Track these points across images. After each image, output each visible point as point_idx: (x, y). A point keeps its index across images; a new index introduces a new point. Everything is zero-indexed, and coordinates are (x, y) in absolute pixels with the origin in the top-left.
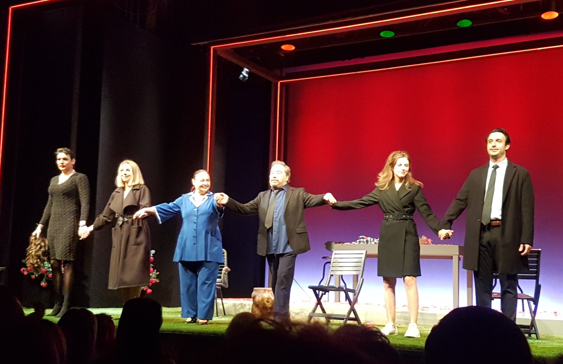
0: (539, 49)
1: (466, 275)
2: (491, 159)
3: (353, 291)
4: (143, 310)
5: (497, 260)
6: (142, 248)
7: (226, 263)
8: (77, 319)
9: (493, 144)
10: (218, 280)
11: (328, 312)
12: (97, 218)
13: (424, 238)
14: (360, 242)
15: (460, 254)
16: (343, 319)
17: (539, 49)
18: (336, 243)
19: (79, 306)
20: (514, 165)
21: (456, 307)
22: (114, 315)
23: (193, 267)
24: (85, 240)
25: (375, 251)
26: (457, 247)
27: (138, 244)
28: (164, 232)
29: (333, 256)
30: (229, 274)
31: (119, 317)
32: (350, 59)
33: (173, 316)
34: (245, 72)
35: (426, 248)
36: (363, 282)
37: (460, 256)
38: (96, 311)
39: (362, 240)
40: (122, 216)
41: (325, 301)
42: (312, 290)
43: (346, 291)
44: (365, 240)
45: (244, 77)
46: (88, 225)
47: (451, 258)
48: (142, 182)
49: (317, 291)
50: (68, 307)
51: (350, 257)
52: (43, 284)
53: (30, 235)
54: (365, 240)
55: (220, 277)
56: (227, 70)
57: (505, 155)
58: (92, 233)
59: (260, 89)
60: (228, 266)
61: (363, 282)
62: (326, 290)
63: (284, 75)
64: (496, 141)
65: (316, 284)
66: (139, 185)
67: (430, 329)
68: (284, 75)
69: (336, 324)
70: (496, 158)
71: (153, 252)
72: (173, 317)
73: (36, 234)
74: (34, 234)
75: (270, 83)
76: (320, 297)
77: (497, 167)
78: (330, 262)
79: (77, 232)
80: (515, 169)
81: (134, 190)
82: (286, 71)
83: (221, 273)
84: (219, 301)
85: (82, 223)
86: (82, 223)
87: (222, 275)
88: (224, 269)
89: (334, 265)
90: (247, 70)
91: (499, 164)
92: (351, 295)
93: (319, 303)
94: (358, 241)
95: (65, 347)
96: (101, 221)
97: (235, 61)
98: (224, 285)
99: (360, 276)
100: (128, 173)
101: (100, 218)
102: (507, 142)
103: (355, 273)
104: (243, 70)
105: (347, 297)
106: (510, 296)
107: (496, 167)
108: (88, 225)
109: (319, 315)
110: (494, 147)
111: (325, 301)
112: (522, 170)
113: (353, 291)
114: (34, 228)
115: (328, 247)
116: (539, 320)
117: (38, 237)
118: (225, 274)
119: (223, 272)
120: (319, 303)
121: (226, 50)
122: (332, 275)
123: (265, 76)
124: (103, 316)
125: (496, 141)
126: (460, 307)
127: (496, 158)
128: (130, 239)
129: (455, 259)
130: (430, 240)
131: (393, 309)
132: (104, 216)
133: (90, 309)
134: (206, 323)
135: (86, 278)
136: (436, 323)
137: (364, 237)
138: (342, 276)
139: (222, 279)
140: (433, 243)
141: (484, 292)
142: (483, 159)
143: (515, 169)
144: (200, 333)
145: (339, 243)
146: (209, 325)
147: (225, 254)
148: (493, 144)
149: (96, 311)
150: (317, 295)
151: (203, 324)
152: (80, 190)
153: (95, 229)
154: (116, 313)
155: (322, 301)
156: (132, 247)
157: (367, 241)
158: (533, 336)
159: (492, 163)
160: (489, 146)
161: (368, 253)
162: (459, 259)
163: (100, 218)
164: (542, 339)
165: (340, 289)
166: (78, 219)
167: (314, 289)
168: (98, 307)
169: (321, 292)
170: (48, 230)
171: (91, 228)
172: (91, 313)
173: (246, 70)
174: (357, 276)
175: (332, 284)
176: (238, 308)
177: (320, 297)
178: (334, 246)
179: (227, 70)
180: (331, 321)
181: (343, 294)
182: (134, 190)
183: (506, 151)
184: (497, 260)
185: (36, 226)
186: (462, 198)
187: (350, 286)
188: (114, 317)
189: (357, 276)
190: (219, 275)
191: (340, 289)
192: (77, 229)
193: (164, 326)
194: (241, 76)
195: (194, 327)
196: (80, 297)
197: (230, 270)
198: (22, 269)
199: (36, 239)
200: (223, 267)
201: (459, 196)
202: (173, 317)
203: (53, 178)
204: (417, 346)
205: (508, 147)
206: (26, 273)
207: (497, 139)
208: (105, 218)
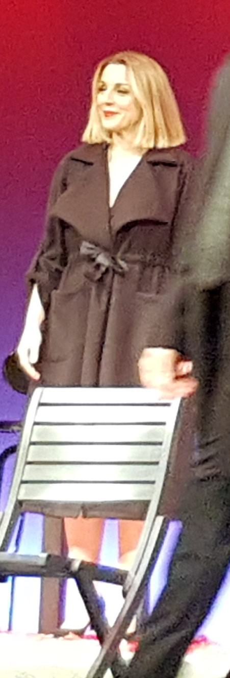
29: (33, 413)
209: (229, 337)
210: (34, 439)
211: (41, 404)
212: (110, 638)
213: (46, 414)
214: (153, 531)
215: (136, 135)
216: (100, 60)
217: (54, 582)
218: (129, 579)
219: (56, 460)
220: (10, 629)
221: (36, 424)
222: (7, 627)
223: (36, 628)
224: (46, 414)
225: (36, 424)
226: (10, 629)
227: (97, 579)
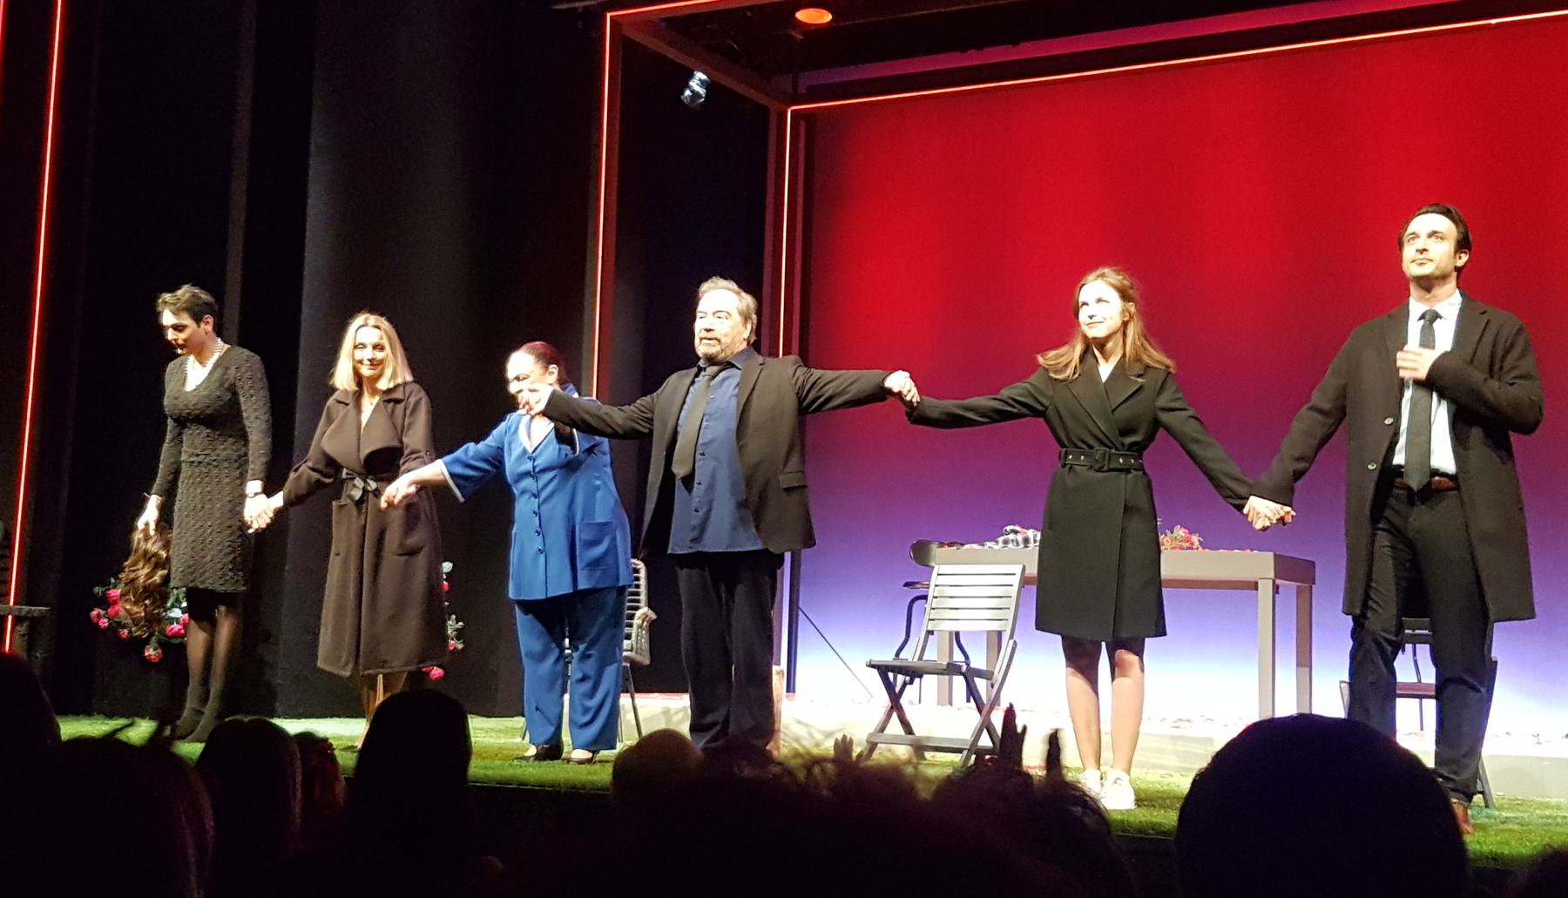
0: (1494, 21)
1: (1294, 633)
2: (1413, 290)
3: (987, 675)
4: (422, 729)
5: (1428, 586)
6: (421, 559)
7: (643, 597)
8: (248, 749)
9: (1419, 243)
10: (626, 644)
11: (919, 731)
12: (292, 475)
13: (1180, 532)
14: (1006, 542)
15: (1278, 575)
16: (959, 751)
17: (1494, 21)
18: (942, 545)
19: (249, 713)
20: (1482, 306)
21: (1267, 715)
22: (340, 738)
23: (557, 616)
24: (260, 534)
25: (1033, 570)
26: (1269, 557)
27: (412, 553)
28: (475, 517)
29: (934, 580)
30: (653, 628)
31: (359, 744)
32: (980, 48)
33: (502, 741)
34: (697, 83)
35: (1181, 556)
36: (1014, 650)
37: (1278, 582)
38: (293, 726)
39: (1011, 536)
40: (360, 475)
41: (911, 703)
42: (875, 671)
43: (970, 675)
44: (1020, 537)
45: (695, 94)
46: (269, 491)
47: (1255, 586)
48: (409, 378)
49: (891, 675)
50: (220, 716)
51: (982, 583)
52: (151, 652)
53: (132, 529)
54: (1020, 537)
55: (628, 637)
56: (650, 78)
57: (1452, 283)
58: (279, 514)
59: (737, 128)
60: (650, 606)
61: (1014, 650)
62: (914, 673)
63: (802, 90)
64: (1430, 241)
65: (887, 657)
66: (405, 384)
67: (1190, 780)
68: (802, 90)
69: (941, 765)
70: (1427, 284)
71: (447, 567)
72: (498, 742)
73: (147, 524)
74: (140, 524)
75: (765, 111)
76: (897, 689)
77: (1436, 316)
78: (925, 597)
79: (241, 513)
80: (1485, 318)
81: (389, 401)
82: (809, 79)
83: (631, 626)
84: (625, 700)
85: (253, 486)
86: (253, 486)
87: (634, 631)
88: (638, 613)
89: (935, 603)
90: (704, 77)
91: (1438, 308)
92: (981, 684)
93: (896, 705)
94: (1001, 539)
95: (210, 824)
96: (304, 482)
97: (672, 54)
98: (638, 658)
99: (1006, 636)
100: (379, 355)
101: (303, 472)
102: (1462, 245)
103: (995, 626)
104: (691, 76)
105: (972, 692)
106: (1464, 692)
107: (1431, 318)
108: (269, 491)
109: (895, 741)
110: (1423, 251)
111: (911, 703)
112: (1506, 321)
113: (987, 675)
114: (140, 507)
115: (921, 554)
116: (1492, 757)
117: (152, 533)
118: (640, 627)
119: (636, 622)
120: (896, 705)
121: (647, 24)
122: (931, 632)
123: (752, 94)
124: (307, 739)
125: (1430, 241)
126: (1278, 715)
127: (1427, 284)
128: (387, 537)
129: (1265, 589)
130: (1195, 539)
131: (1094, 729)
132: (313, 470)
133: (278, 722)
134: (589, 761)
135: (267, 637)
136: (1204, 763)
137: (1018, 528)
138: (957, 634)
139: (635, 643)
140: (1204, 545)
141: (1372, 684)
142: (1389, 291)
143: (1485, 318)
144: (574, 787)
145: (951, 545)
146: (598, 766)
147: (643, 574)
148: (1419, 243)
149: (293, 726)
150: (889, 686)
151: (581, 762)
152: (242, 399)
153: (289, 503)
154: (346, 733)
155: (903, 701)
156: (391, 560)
157: (1026, 541)
158: (1478, 798)
159: (1416, 307)
160: (1409, 252)
161: (1027, 571)
162: (1276, 589)
163: (303, 472)
164: (1501, 808)
165: (952, 669)
166: (242, 479)
167: (883, 670)
168: (299, 716)
169: (900, 678)
170: (176, 508)
171: (278, 500)
172: (281, 732)
173: (700, 75)
174: (1000, 633)
175: (931, 655)
176: (675, 719)
177: (897, 689)
178: (937, 552)
179: (650, 78)
180: (928, 755)
181: (959, 682)
182: (389, 401)
183: (1458, 269)
184: (1428, 586)
185: (145, 500)
186: (1326, 406)
187: (979, 661)
188: (335, 743)
189: (1000, 633)
190: (627, 630)
191: (952, 669)
192: (242, 504)
193: (476, 768)
194: (688, 93)
195: (551, 772)
196: (251, 685)
197: (654, 617)
198: (94, 613)
199: (147, 538)
200: (637, 608)
201: (1316, 398)
202: (498, 742)
203: (171, 365)
204: (1160, 824)
205: (1465, 258)
206: (104, 623)
207: (1430, 230)
208: (316, 476)
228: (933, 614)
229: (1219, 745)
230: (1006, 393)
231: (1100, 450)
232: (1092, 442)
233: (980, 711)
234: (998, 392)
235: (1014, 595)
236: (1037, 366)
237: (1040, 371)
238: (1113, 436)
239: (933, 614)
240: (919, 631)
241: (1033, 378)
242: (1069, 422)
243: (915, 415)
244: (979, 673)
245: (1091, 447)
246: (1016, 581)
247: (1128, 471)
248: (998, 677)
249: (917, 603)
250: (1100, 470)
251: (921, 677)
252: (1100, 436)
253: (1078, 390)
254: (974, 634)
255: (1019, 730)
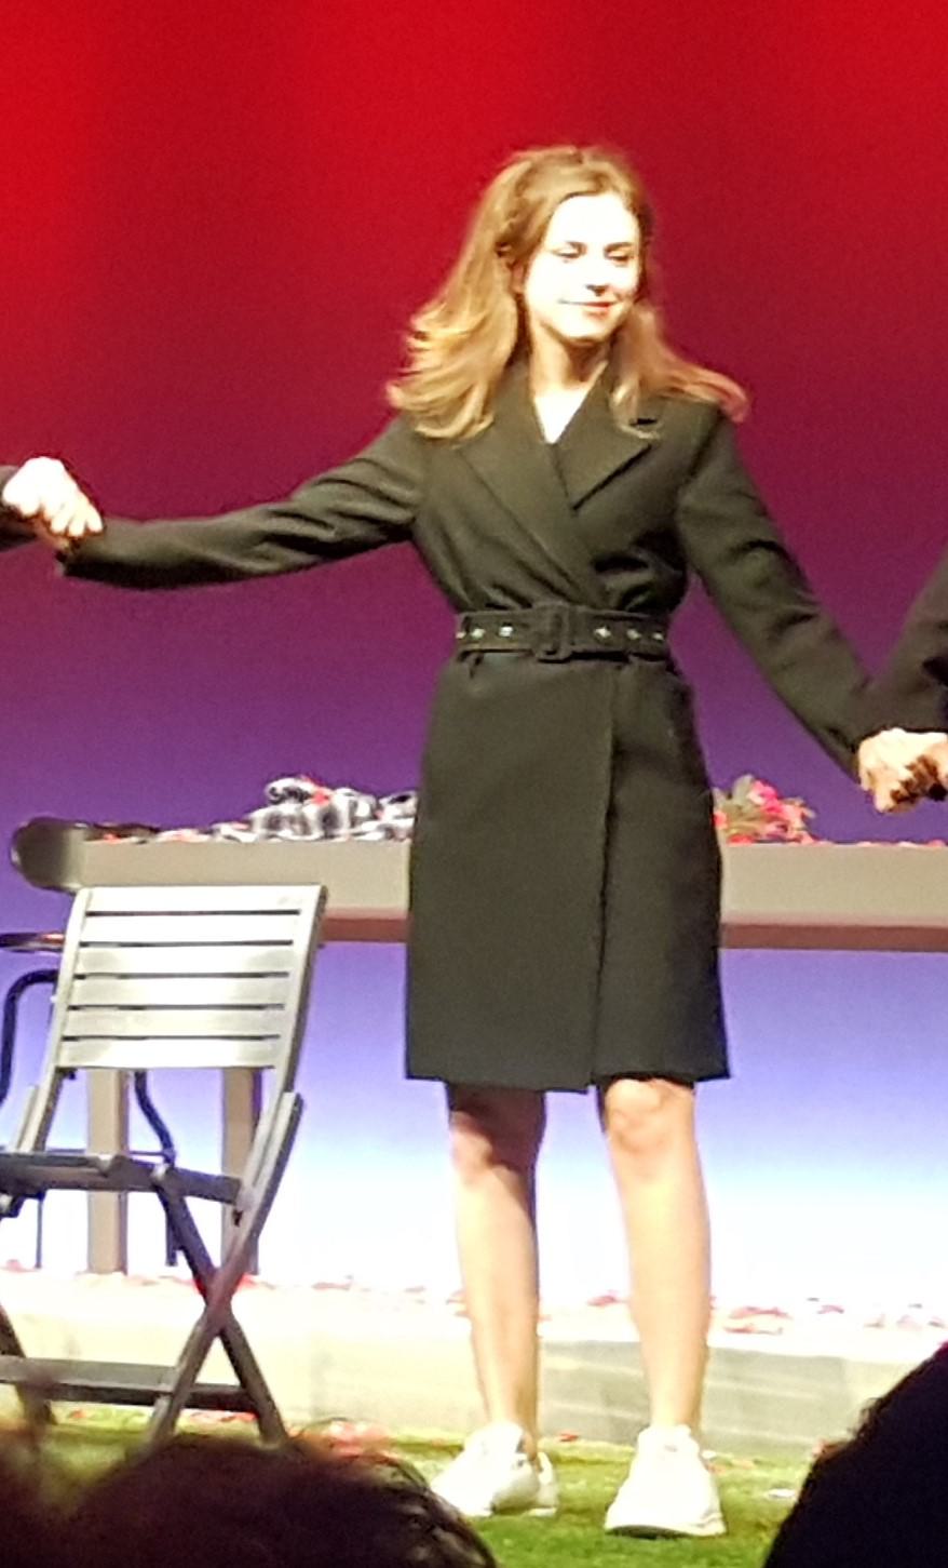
3: (221, 1190)
13: (750, 794)
16: (147, 1399)
18: (98, 831)
29: (77, 929)
35: (769, 868)
39: (288, 808)
43: (175, 1189)
44: (311, 811)
54: (311, 811)
67: (799, 1474)
78: (50, 977)
89: (80, 992)
92: (206, 1216)
94: (260, 815)
99: (273, 1082)
103: (235, 1055)
105: (181, 1238)
113: (221, 1190)
122: (66, 1073)
130: (793, 812)
131: (518, 1322)
136: (842, 1430)
137: (307, 786)
140: (816, 831)
145: (122, 832)
165: (124, 1175)
174: (256, 1075)
175: (67, 1137)
178: (86, 851)
180: (62, 1411)
181: (146, 1210)
187: (200, 1154)
189: (256, 1075)
191: (124, 1175)
209: (341, 799)
210: (81, 970)
211: (91, 914)
212: (216, 1286)
213: (99, 929)
214: (281, 1111)
215: (453, 363)
216: (523, 145)
217: (109, 1198)
218: (243, 1193)
219: (314, 995)
220: (38, 1265)
221: (84, 945)
222: (33, 1261)
223: (84, 1266)
224: (99, 929)
225: (84, 945)
226: (38, 1265)
227: (193, 1194)
228: (75, 1023)
229: (883, 1386)
230: (308, 497)
231: (548, 604)
232: (525, 588)
233: (203, 1290)
234: (285, 495)
235: (297, 970)
236: (392, 412)
237: (394, 428)
238: (582, 570)
239: (75, 1023)
240: (37, 1070)
241: (377, 450)
242: (461, 537)
243: (84, 561)
244: (205, 1187)
245: (525, 603)
246: (300, 931)
247: (619, 657)
248: (253, 1194)
249: (36, 988)
250: (551, 658)
251: (40, 1196)
252: (543, 569)
253: (486, 462)
254: (181, 1076)
255: (181, 1257)
